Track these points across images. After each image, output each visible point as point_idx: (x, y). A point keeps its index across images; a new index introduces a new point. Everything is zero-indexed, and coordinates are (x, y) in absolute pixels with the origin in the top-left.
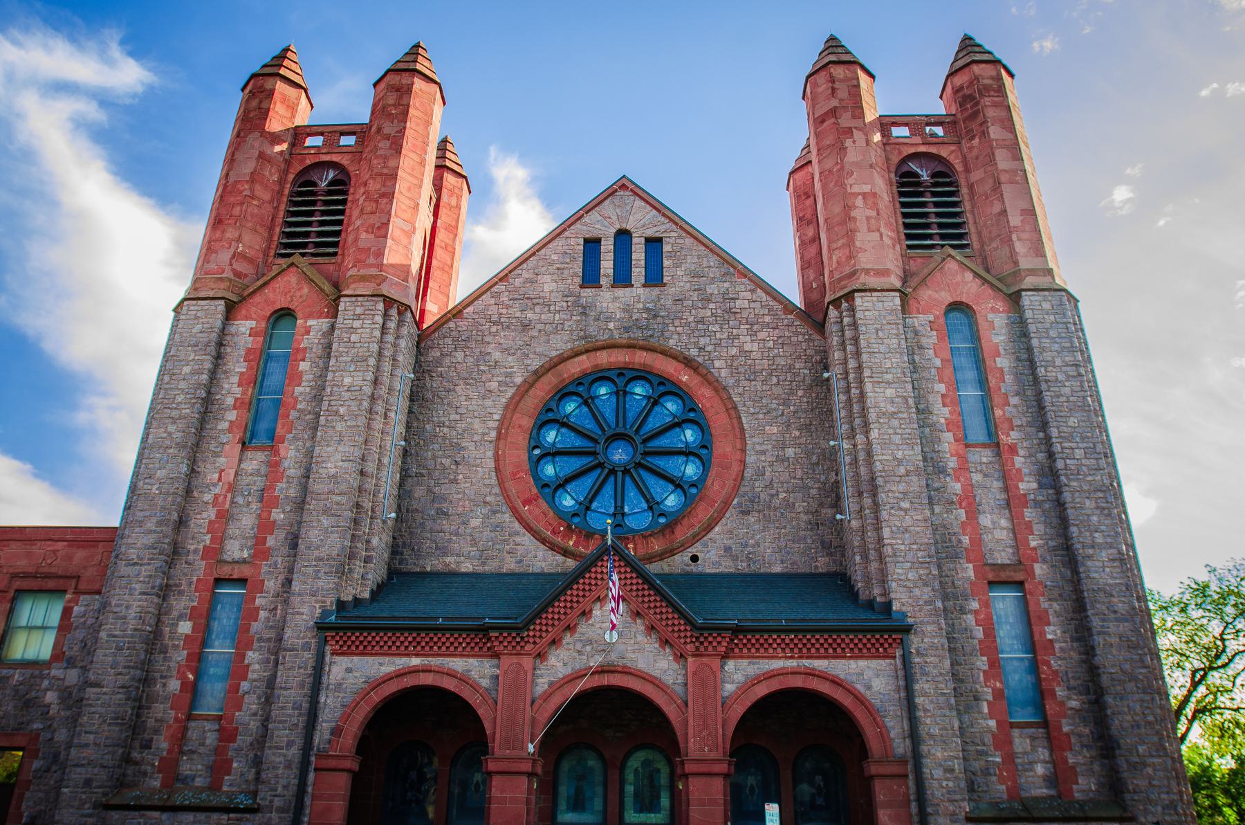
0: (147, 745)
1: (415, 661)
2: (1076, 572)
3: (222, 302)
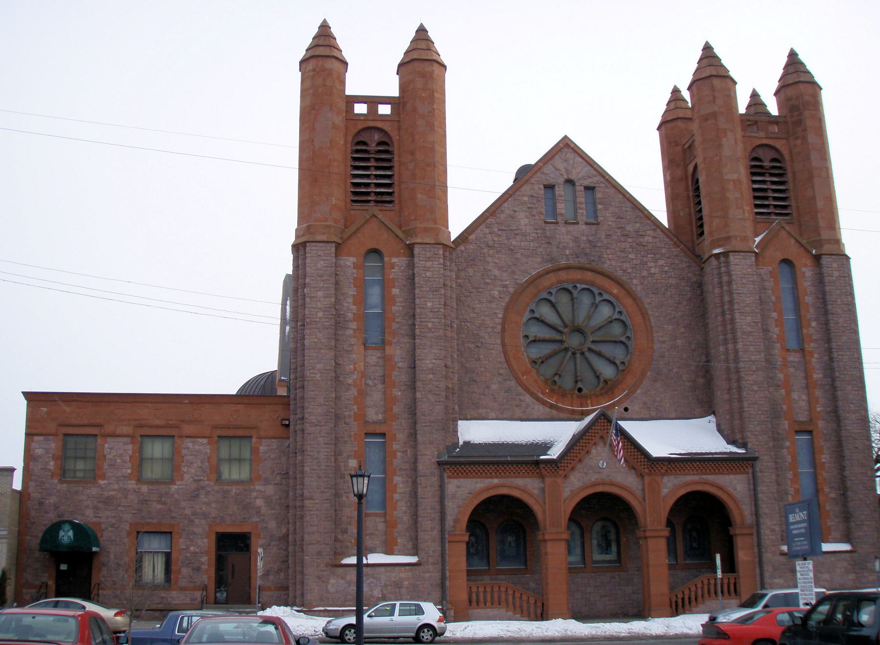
0: (345, 531)
1: (496, 481)
2: (839, 426)
3: (334, 245)
